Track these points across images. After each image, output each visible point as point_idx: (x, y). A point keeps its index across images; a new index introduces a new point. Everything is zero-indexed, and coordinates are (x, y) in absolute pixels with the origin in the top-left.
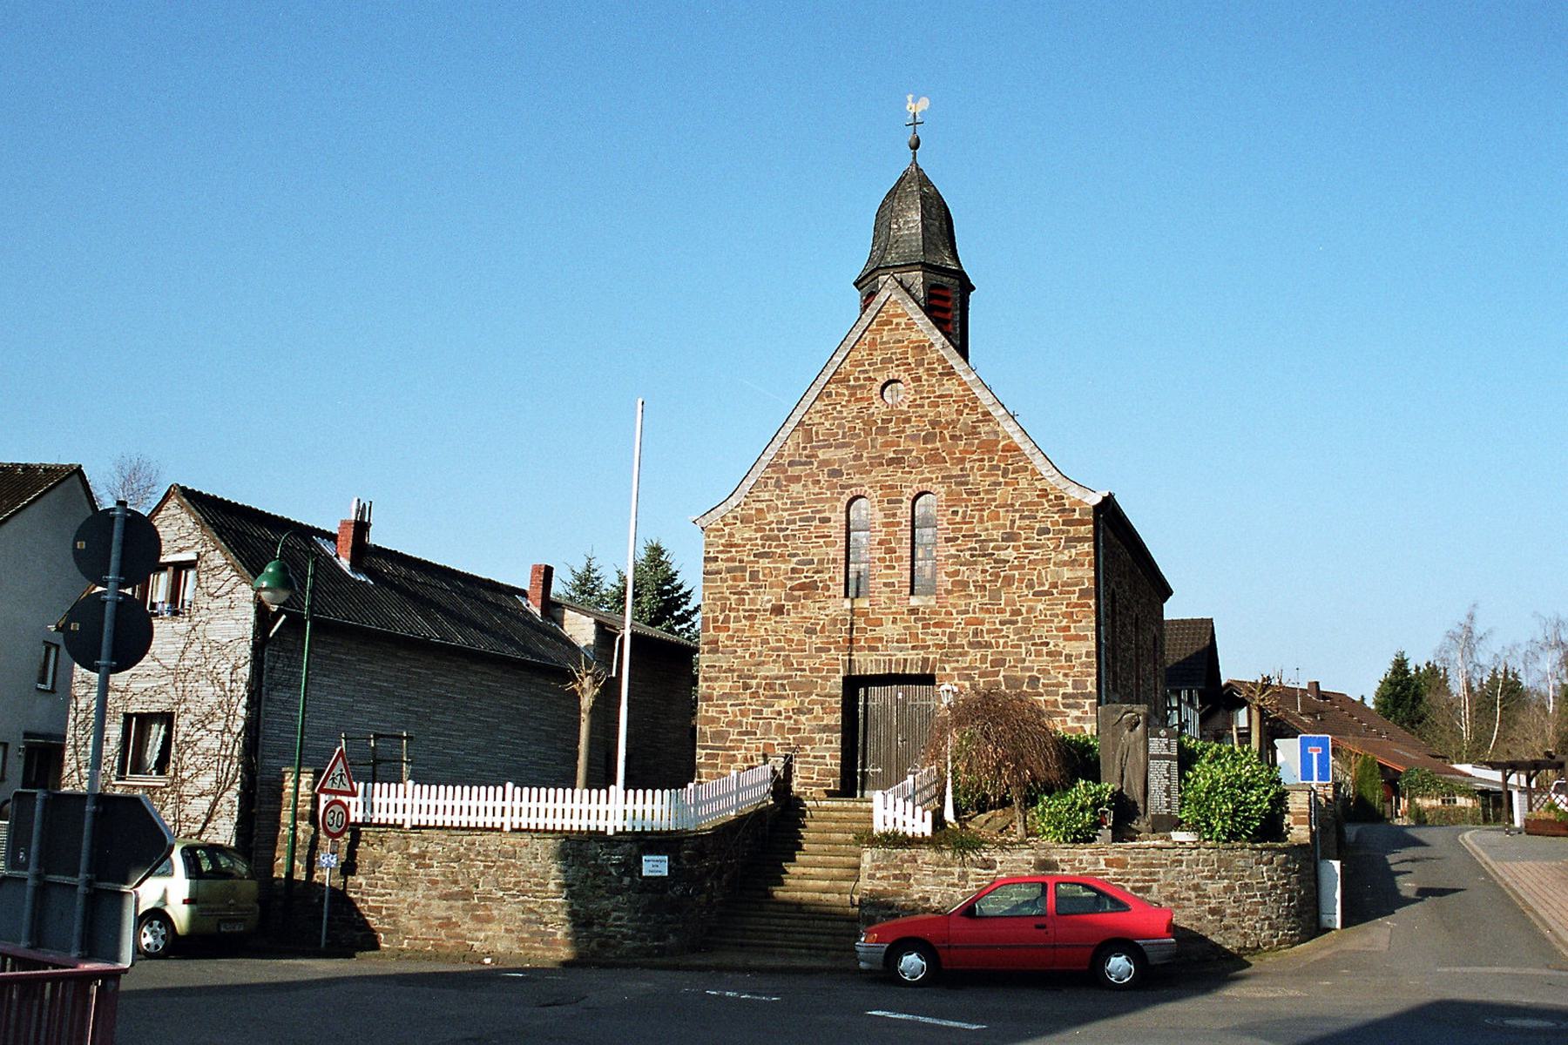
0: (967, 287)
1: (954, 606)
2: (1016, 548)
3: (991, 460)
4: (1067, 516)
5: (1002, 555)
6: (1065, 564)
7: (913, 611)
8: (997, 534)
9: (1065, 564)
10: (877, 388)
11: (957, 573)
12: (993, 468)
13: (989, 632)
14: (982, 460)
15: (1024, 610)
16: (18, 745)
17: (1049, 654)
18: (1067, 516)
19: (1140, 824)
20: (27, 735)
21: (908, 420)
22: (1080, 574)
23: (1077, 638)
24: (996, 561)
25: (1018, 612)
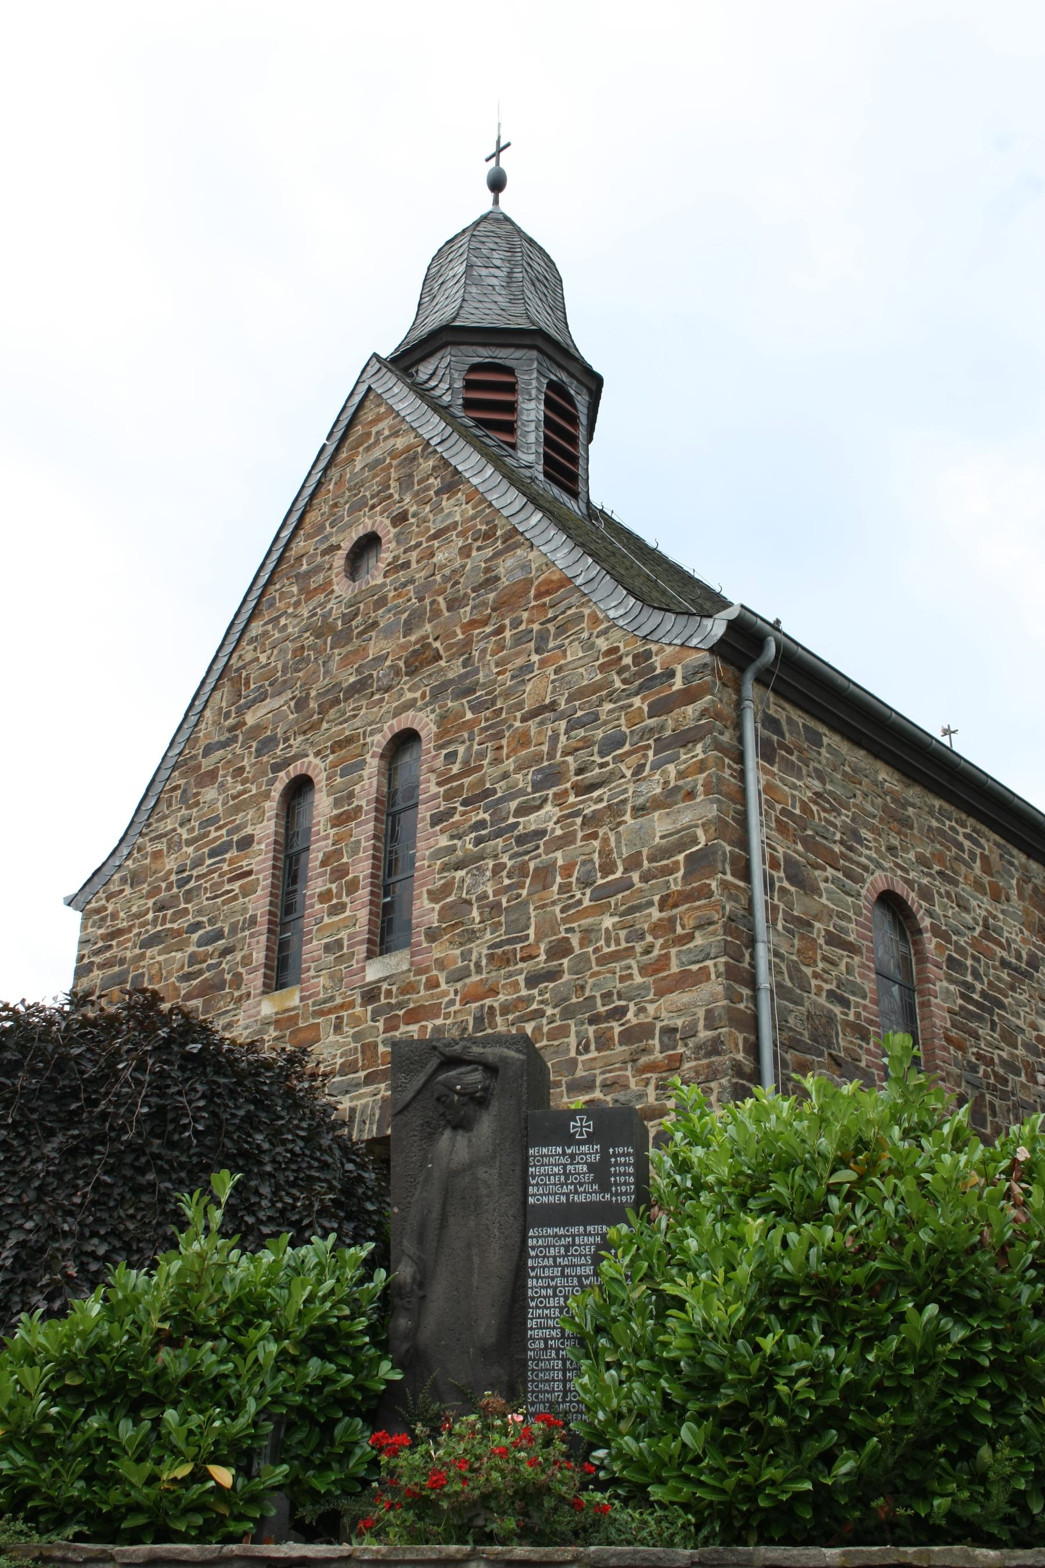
0: (594, 383)
1: (441, 964)
2: (560, 799)
3: (516, 623)
4: (660, 693)
5: (532, 822)
6: (657, 804)
7: (371, 995)
8: (523, 780)
9: (657, 804)
10: (339, 560)
11: (446, 889)
12: (519, 640)
13: (505, 1010)
14: (500, 630)
15: (575, 940)
16: (731, 613)
17: (628, 1036)
18: (660, 693)
19: (851, 1215)
20: (742, 606)
21: (382, 602)
22: (686, 819)
23: (686, 980)
24: (521, 840)
25: (560, 949)
